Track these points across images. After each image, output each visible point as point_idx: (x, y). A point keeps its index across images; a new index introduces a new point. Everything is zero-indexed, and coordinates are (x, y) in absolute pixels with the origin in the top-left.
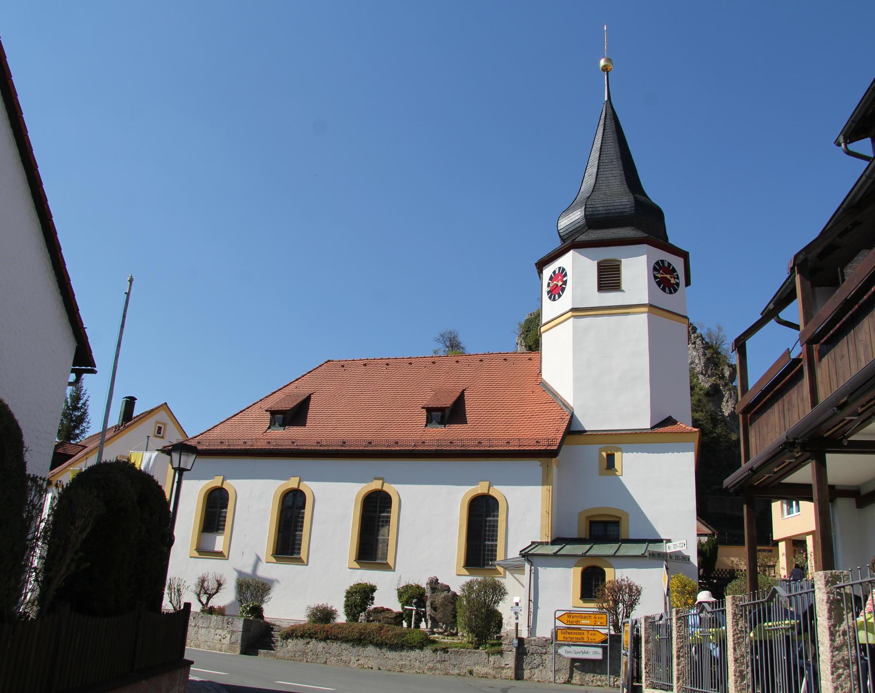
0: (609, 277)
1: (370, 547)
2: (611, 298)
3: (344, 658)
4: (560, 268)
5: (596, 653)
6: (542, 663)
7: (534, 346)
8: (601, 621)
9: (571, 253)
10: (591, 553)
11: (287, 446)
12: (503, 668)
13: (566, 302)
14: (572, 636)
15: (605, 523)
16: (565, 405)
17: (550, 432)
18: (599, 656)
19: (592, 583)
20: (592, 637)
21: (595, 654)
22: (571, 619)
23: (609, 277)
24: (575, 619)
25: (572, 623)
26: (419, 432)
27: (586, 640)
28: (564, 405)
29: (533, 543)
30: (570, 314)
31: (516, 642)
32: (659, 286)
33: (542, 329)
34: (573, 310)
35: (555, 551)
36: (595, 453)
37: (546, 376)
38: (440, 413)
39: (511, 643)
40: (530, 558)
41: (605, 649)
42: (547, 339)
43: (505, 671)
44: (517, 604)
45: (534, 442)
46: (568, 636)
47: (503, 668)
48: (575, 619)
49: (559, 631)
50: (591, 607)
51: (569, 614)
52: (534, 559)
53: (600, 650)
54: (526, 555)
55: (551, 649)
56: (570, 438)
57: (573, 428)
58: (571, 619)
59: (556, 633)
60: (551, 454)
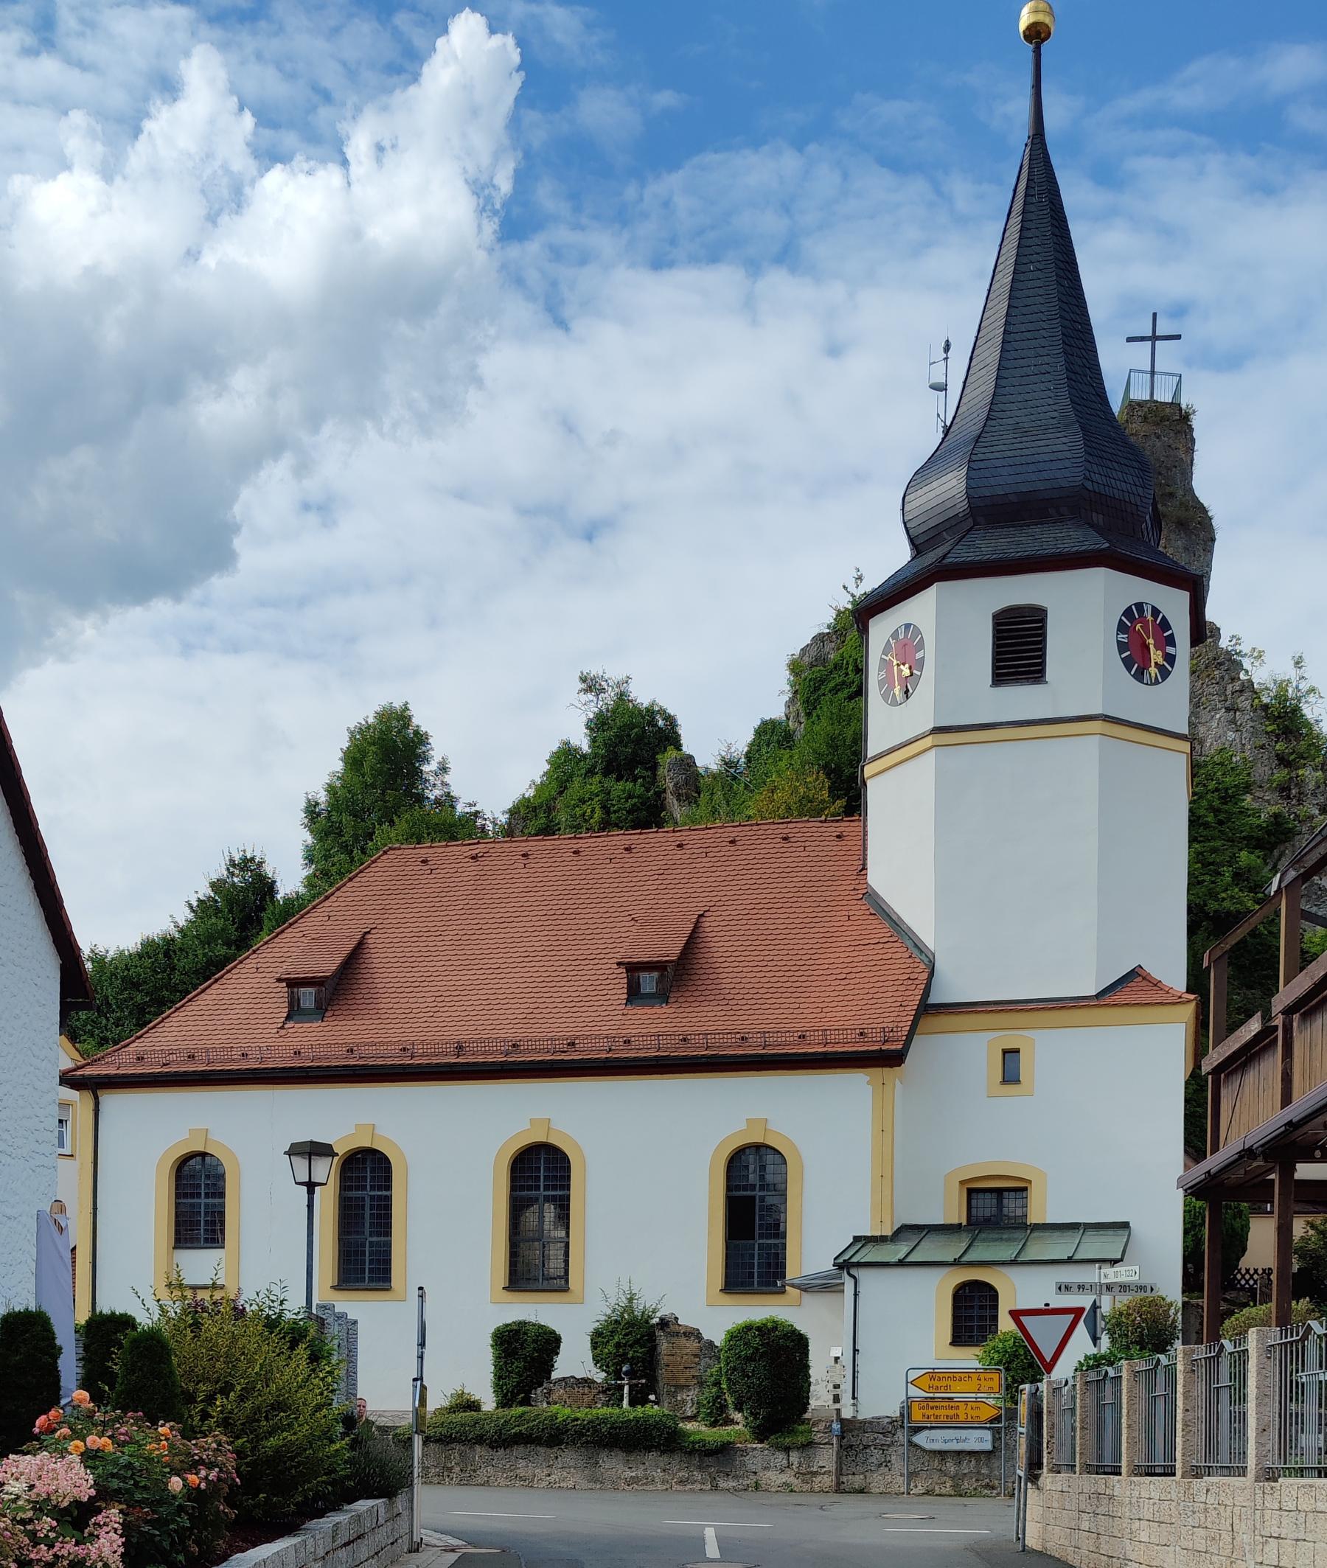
0: (1019, 648)
1: (533, 1259)
2: (1021, 701)
3: (521, 1472)
4: (907, 626)
5: (981, 1440)
6: (887, 1464)
7: (848, 794)
8: (990, 1384)
9: (933, 590)
10: (970, 1257)
11: (337, 1058)
12: (815, 1474)
13: (920, 713)
14: (937, 1412)
15: (999, 1192)
16: (919, 947)
17: (884, 1015)
18: (988, 1446)
19: (972, 1313)
20: (974, 1413)
21: (979, 1440)
22: (936, 1383)
23: (1019, 648)
24: (944, 1383)
25: (937, 1390)
26: (609, 1020)
27: (962, 1419)
28: (916, 945)
29: (857, 1239)
30: (928, 741)
31: (836, 1426)
32: (1129, 670)
33: (869, 770)
34: (937, 730)
35: (901, 1256)
36: (973, 1050)
37: (877, 878)
38: (655, 975)
39: (829, 1429)
40: (853, 1271)
41: (996, 1432)
42: (880, 792)
43: (819, 1478)
44: (837, 1359)
45: (854, 1036)
46: (930, 1412)
47: (815, 1474)
48: (944, 1383)
49: (915, 1406)
50: (968, 1358)
51: (933, 1374)
52: (861, 1274)
53: (988, 1435)
54: (844, 1265)
55: (902, 1436)
56: (926, 1022)
57: (933, 1000)
58: (936, 1383)
59: (909, 1408)
60: (892, 1059)
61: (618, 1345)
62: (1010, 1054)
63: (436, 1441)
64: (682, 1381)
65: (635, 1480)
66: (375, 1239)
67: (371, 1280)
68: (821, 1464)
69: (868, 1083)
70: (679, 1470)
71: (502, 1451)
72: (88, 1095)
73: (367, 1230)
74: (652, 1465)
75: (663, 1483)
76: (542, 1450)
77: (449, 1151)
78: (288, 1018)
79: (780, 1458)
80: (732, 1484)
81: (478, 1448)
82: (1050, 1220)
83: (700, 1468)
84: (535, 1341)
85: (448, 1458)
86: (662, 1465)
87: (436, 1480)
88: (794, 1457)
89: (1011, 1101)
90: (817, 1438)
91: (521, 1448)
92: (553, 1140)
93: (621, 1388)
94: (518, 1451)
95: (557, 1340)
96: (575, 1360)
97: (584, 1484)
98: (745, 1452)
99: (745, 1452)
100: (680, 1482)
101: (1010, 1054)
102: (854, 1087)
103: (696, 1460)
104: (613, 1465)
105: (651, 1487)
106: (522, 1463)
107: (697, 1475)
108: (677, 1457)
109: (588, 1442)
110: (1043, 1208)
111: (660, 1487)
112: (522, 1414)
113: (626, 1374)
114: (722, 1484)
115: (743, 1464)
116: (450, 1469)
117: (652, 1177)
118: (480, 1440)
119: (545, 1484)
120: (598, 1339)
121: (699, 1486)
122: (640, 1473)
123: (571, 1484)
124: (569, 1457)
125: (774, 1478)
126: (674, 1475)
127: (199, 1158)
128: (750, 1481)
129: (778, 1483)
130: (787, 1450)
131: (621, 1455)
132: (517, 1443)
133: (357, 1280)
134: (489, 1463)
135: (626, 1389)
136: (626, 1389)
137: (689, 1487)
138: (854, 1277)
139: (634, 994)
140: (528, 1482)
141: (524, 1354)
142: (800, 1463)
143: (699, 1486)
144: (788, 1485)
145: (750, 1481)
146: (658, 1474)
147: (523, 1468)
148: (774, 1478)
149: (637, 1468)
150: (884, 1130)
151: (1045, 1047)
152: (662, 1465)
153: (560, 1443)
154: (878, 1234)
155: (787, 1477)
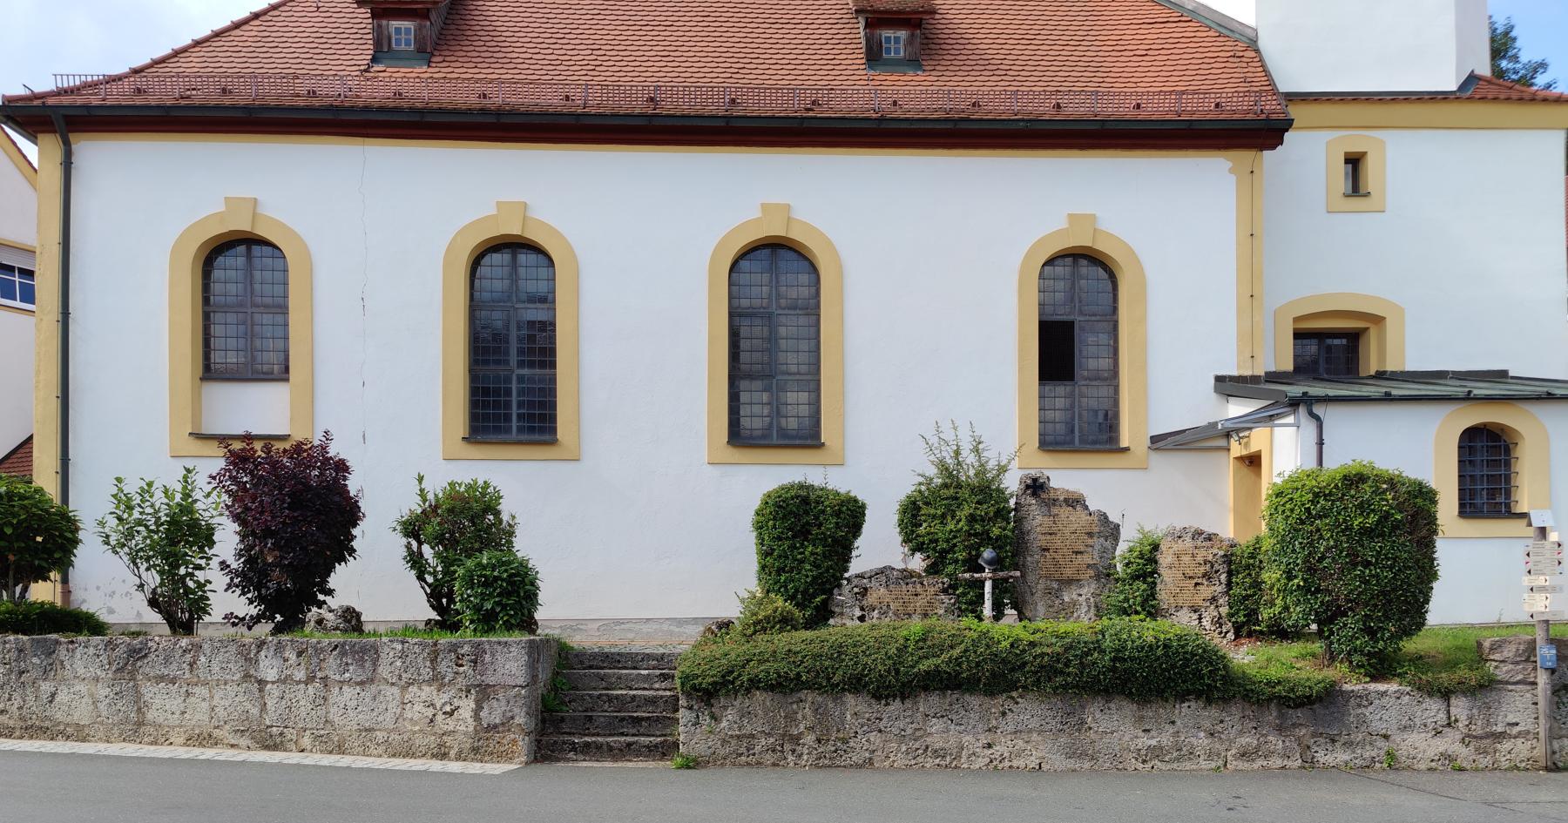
3: (936, 742)
12: (1499, 737)
40: (1318, 410)
43: (1507, 745)
47: (1499, 737)
61: (972, 519)
62: (1354, 162)
63: (771, 688)
64: (1068, 573)
65: (1157, 752)
66: (525, 371)
67: (520, 430)
68: (1511, 718)
69: (1231, 171)
70: (1241, 733)
71: (896, 705)
72: (52, 142)
73: (514, 358)
74: (1189, 724)
75: (1210, 757)
76: (974, 701)
77: (641, 248)
78: (374, 60)
79: (1433, 709)
80: (1341, 756)
81: (850, 699)
82: (1411, 366)
83: (1279, 729)
84: (838, 514)
85: (791, 718)
86: (1207, 724)
87: (769, 758)
88: (1460, 707)
89: (1356, 224)
90: (1502, 672)
91: (934, 699)
92: (796, 235)
93: (981, 583)
94: (929, 703)
95: (863, 507)
96: (879, 547)
97: (1059, 762)
98: (1364, 699)
99: (1364, 699)
100: (1243, 755)
101: (1354, 162)
102: (1208, 177)
103: (1272, 715)
104: (1115, 726)
105: (1188, 765)
106: (936, 726)
107: (1276, 742)
108: (1236, 710)
109: (1065, 687)
110: (1378, 356)
111: (1204, 764)
112: (822, 628)
113: (990, 563)
114: (1321, 757)
115: (1362, 721)
116: (796, 740)
117: (929, 288)
118: (856, 684)
119: (980, 763)
120: (911, 514)
121: (1279, 762)
122: (1166, 739)
123: (1033, 764)
124: (1029, 711)
125: (1421, 746)
126: (1232, 742)
127: (242, 249)
128: (1378, 749)
129: (1431, 753)
130: (1446, 695)
131: (1129, 708)
132: (926, 689)
133: (497, 430)
134: (874, 725)
135: (988, 586)
136: (988, 586)
137: (1260, 763)
138: (1318, 418)
139: (874, 56)
140: (948, 761)
141: (807, 536)
142: (1470, 718)
143: (1279, 762)
144: (1448, 757)
145: (1378, 749)
146: (1201, 741)
147: (938, 733)
148: (1422, 745)
149: (1160, 731)
150: (1251, 236)
151: (1400, 156)
152: (1207, 724)
153: (1013, 686)
154: (1248, 373)
155: (1450, 743)
